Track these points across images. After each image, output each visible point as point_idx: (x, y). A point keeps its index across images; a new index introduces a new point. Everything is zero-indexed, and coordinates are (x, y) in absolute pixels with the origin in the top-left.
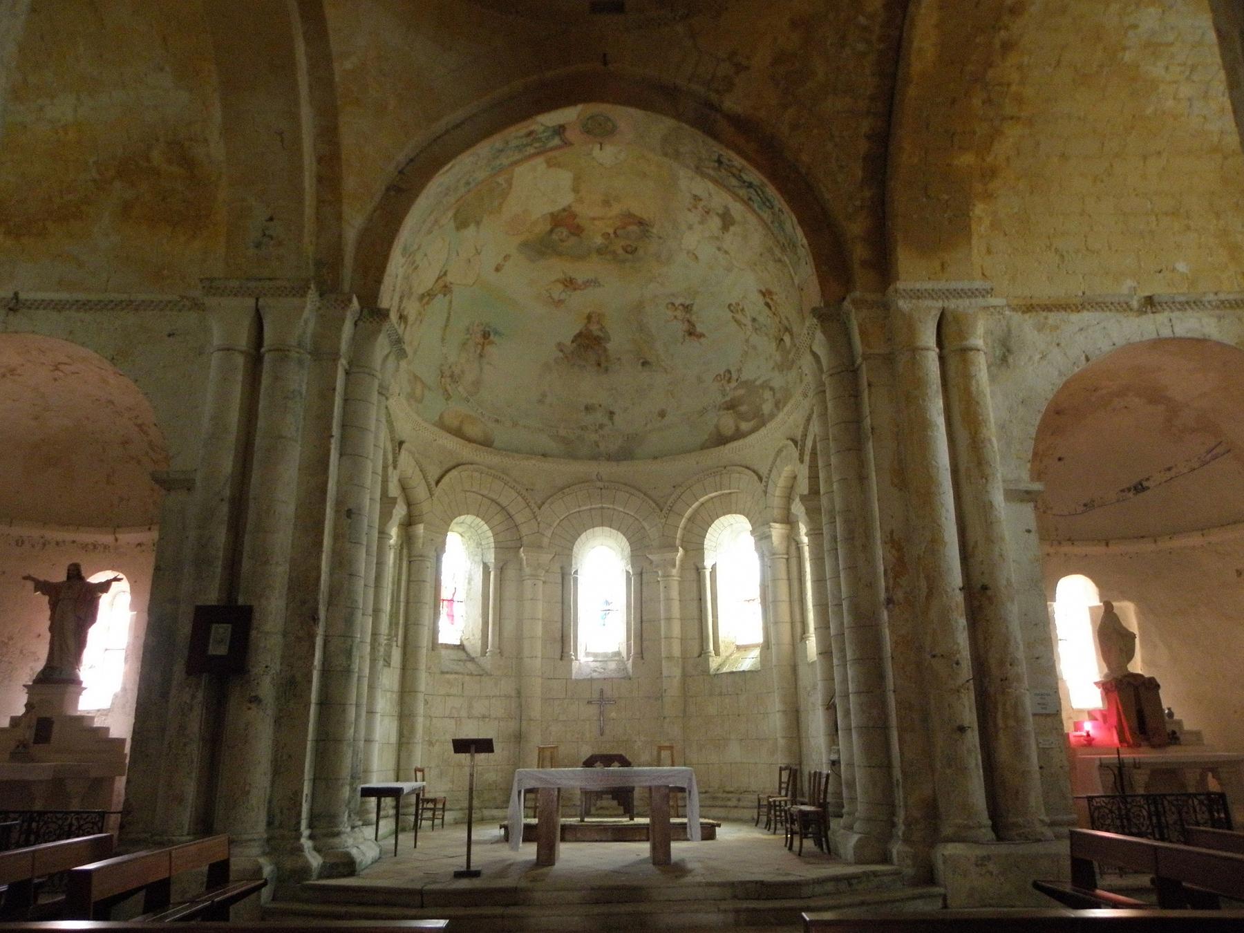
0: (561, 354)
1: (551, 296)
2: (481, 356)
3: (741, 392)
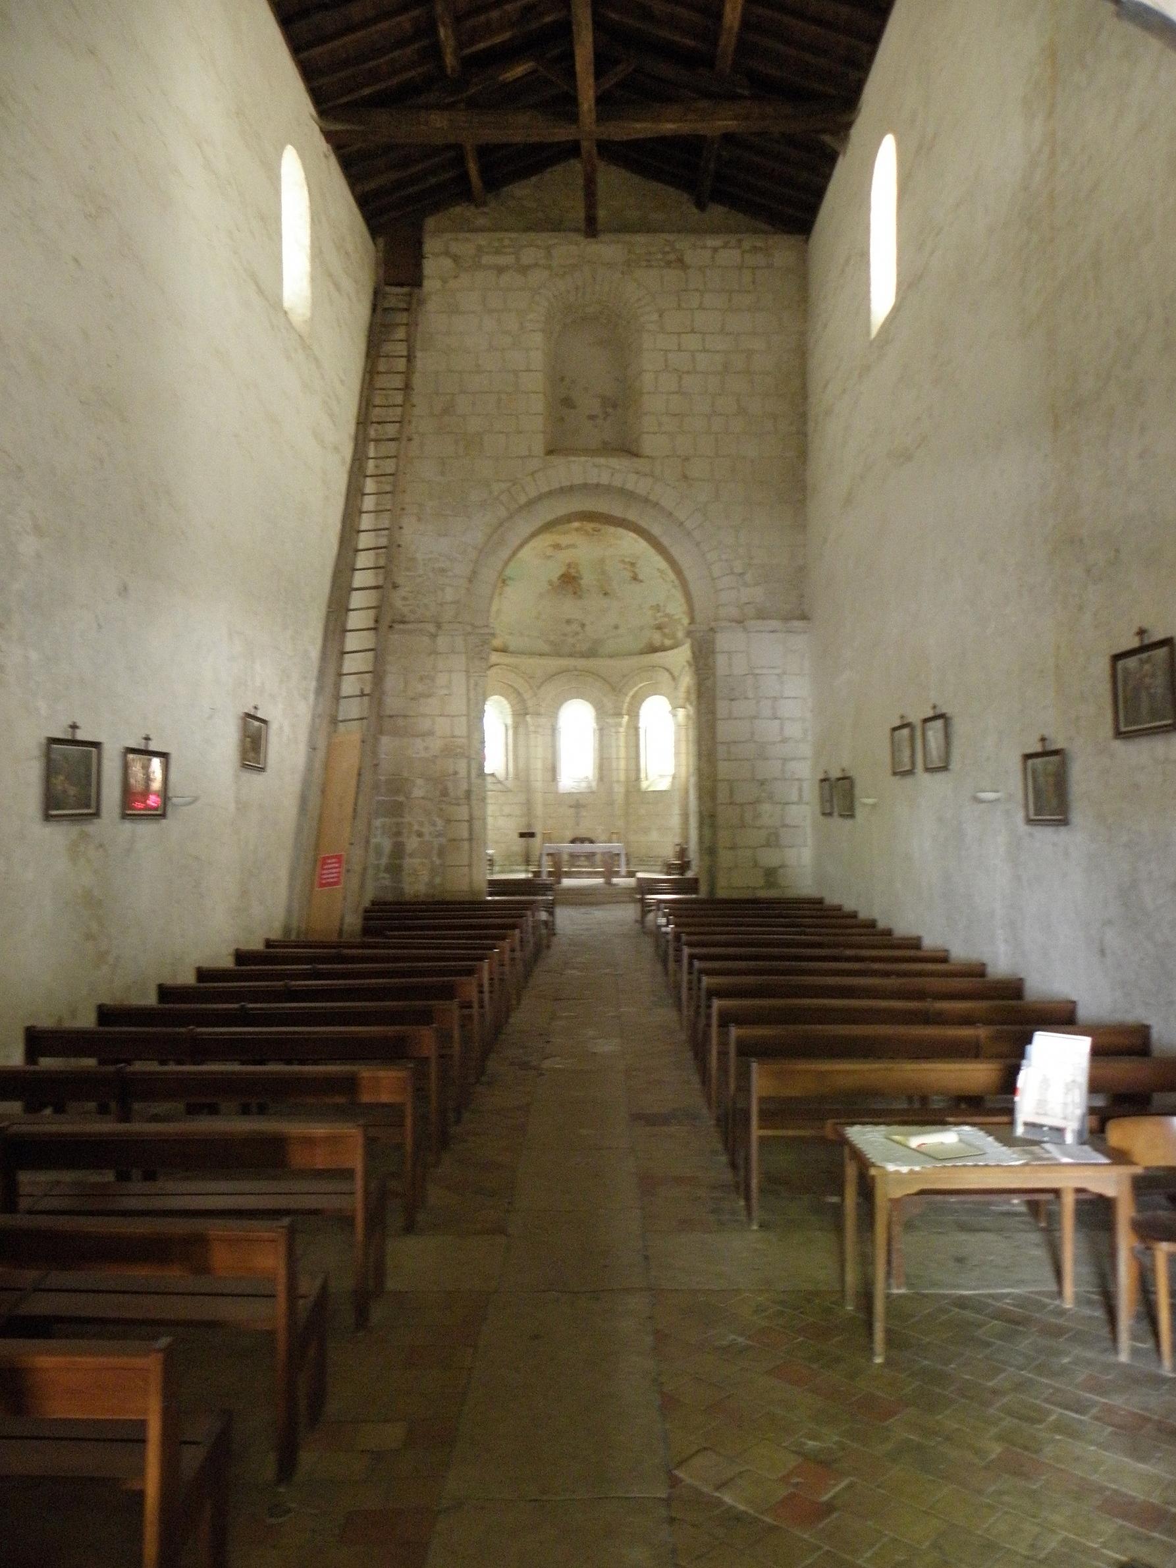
0: (550, 587)
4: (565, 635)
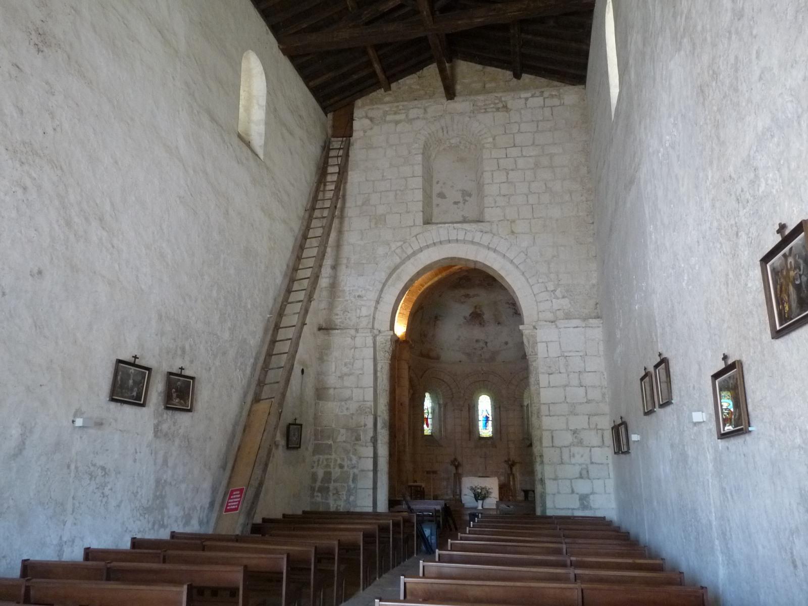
4: (475, 349)
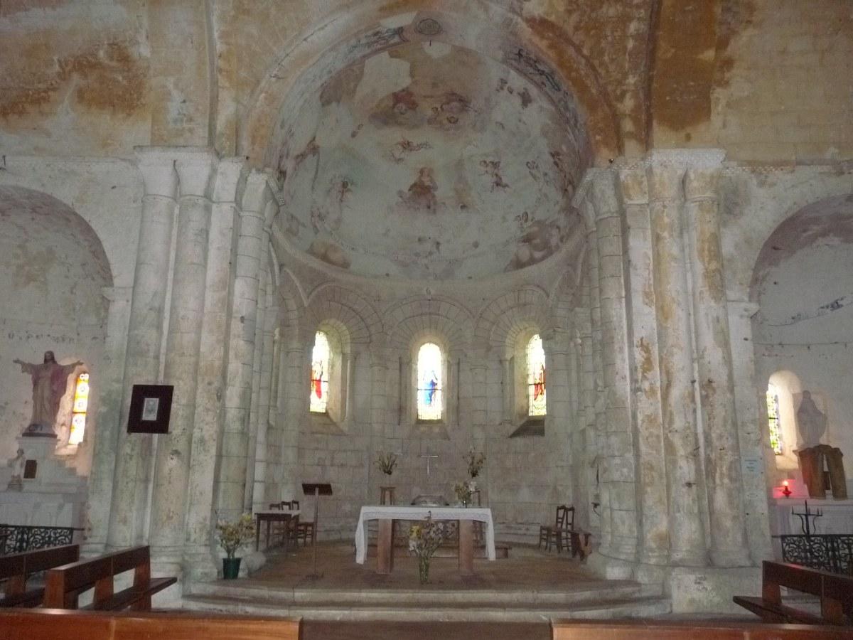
0: (400, 200)
1: (393, 155)
2: (341, 201)
3: (535, 229)
4: (417, 255)
